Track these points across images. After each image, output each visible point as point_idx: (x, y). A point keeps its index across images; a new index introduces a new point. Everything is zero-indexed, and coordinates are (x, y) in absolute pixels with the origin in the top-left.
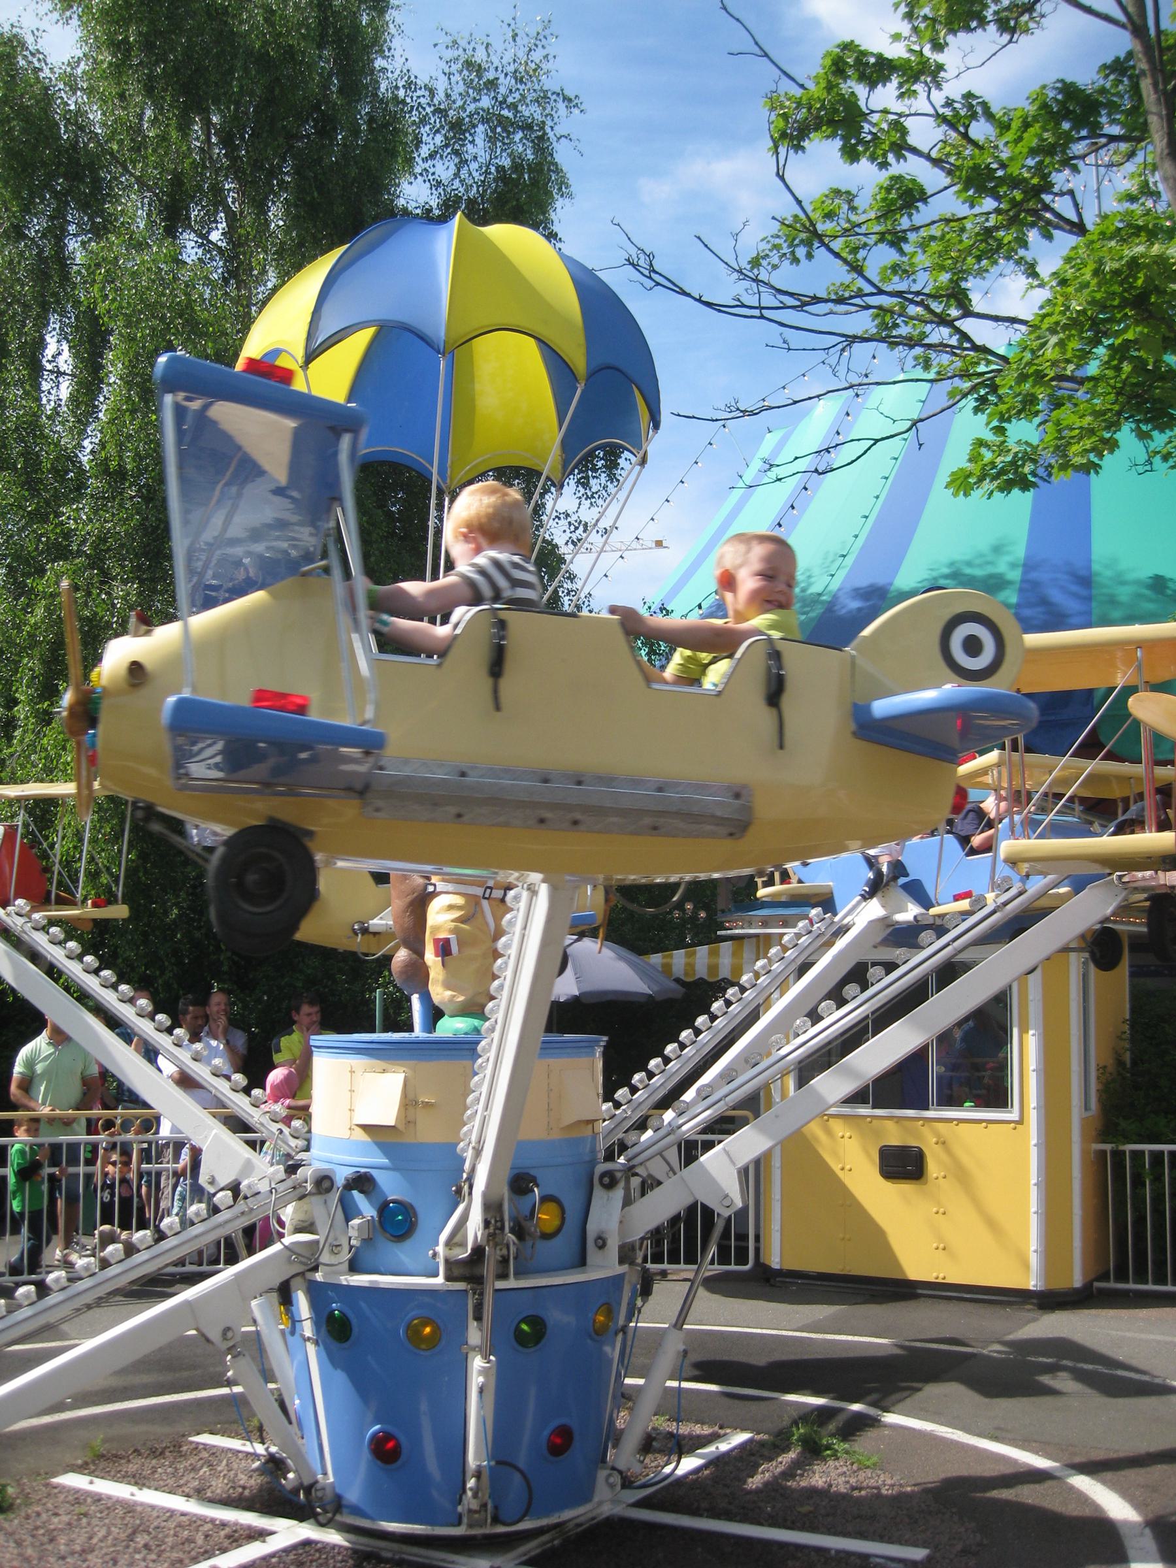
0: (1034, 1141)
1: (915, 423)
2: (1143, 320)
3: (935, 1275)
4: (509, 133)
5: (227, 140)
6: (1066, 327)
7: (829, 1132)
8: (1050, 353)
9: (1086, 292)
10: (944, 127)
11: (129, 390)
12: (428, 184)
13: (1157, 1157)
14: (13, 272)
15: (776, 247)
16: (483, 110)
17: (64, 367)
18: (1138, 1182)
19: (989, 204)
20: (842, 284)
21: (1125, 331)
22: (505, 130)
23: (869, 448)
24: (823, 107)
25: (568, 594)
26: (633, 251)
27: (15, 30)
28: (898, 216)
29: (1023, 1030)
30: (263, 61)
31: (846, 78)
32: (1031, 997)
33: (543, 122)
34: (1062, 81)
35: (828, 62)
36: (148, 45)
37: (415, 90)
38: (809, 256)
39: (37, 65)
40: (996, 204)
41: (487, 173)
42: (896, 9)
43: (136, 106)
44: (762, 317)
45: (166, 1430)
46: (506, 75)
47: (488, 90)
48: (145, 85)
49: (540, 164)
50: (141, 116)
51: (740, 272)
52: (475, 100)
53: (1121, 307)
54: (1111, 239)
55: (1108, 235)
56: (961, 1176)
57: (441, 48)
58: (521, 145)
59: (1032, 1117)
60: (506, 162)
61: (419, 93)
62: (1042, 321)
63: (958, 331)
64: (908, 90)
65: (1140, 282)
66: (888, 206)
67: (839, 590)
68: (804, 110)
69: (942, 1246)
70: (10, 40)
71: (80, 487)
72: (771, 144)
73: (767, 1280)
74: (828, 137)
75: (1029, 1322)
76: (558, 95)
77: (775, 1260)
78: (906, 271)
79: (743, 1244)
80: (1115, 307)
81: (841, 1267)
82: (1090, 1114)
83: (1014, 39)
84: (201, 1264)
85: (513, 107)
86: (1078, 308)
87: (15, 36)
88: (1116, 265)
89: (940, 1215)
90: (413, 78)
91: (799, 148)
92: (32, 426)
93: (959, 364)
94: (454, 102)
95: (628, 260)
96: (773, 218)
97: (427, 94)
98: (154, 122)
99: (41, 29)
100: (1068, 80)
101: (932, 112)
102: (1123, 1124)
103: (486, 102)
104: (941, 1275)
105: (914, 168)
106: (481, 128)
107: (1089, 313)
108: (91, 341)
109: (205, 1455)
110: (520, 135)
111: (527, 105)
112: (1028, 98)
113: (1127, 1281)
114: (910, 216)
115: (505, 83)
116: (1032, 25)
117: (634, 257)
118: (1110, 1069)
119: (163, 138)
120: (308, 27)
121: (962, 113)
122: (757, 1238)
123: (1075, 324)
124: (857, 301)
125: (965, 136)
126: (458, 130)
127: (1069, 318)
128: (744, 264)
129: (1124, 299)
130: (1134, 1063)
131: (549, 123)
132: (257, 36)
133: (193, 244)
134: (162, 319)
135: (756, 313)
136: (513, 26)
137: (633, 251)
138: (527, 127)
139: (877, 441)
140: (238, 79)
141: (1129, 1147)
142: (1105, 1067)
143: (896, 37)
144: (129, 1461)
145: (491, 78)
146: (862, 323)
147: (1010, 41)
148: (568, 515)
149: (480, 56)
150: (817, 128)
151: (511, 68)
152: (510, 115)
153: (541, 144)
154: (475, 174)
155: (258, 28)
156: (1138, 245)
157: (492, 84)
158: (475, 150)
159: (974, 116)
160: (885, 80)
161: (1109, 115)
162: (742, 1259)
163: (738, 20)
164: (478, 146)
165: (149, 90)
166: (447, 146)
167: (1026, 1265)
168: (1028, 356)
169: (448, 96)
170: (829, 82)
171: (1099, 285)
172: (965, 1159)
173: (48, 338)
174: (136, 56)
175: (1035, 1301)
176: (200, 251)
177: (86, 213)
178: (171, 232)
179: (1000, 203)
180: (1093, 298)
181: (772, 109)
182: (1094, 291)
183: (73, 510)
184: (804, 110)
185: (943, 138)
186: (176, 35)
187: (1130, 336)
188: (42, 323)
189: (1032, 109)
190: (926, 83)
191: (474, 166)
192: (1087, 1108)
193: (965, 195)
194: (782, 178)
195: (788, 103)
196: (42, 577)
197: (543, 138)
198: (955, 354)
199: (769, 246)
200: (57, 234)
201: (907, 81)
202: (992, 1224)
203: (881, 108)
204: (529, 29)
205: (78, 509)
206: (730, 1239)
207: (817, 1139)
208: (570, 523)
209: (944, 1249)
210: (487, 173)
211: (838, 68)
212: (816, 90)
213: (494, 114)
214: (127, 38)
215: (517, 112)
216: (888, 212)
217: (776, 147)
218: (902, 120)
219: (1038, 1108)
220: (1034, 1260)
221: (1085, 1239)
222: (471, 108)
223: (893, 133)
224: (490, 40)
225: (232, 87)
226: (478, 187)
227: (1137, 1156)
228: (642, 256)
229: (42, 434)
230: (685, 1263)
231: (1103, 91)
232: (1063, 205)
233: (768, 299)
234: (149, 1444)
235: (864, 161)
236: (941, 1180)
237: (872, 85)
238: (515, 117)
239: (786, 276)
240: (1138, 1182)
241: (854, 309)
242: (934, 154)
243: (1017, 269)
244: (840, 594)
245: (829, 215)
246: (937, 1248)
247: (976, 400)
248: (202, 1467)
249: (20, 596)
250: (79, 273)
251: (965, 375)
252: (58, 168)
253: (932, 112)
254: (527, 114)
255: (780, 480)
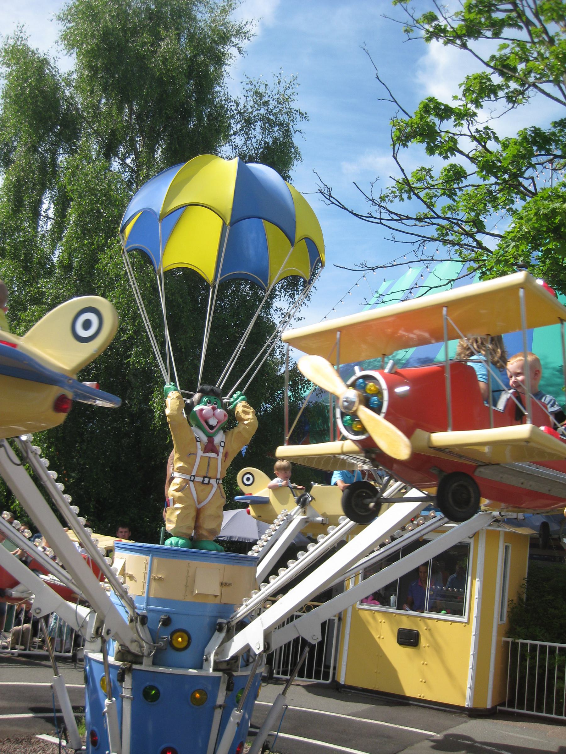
0: (473, 633)
1: (450, 281)
2: (557, 238)
3: (419, 695)
4: (272, 127)
5: (139, 118)
6: (519, 239)
7: (374, 619)
8: (510, 250)
9: (530, 223)
10: (475, 143)
11: (77, 228)
12: (231, 147)
13: (534, 647)
14: (30, 167)
15: (393, 192)
16: (261, 115)
17: (51, 215)
18: (523, 659)
19: (492, 180)
20: (423, 213)
21: (549, 243)
22: (270, 125)
23: (427, 291)
24: (418, 127)
25: (279, 347)
26: (322, 186)
27: (45, 57)
28: (452, 184)
29: (473, 578)
30: (160, 82)
31: (430, 114)
32: (478, 562)
33: (289, 124)
34: (534, 127)
35: (422, 106)
36: (106, 69)
37: (230, 102)
38: (409, 198)
39: (54, 73)
40: (496, 180)
41: (260, 144)
42: (460, 87)
43: (97, 96)
44: (381, 223)
45: (26, 730)
46: (273, 99)
47: (264, 106)
48: (103, 87)
49: (286, 143)
50: (99, 102)
51: (373, 201)
52: (257, 110)
53: (547, 232)
54: (546, 200)
55: (545, 198)
56: (437, 648)
57: (244, 84)
58: (277, 133)
59: (474, 621)
60: (270, 141)
61: (232, 104)
62: (508, 235)
63: (476, 240)
64: (459, 122)
65: (557, 221)
66: (448, 178)
67: (410, 358)
68: (409, 128)
69: (424, 681)
70: (42, 60)
71: (50, 273)
72: (392, 143)
73: (337, 689)
74: (420, 142)
75: (463, 723)
76: (297, 111)
77: (342, 680)
78: (454, 210)
79: (327, 670)
80: (544, 231)
81: (374, 686)
82: (502, 622)
83: (515, 107)
84: (61, 652)
85: (275, 115)
86: (526, 230)
87: (45, 59)
88: (546, 211)
89: (424, 665)
90: (229, 97)
91: (405, 145)
92: (30, 242)
93: (473, 255)
94: (248, 109)
95: (319, 190)
96: (390, 177)
97: (235, 105)
98: (106, 104)
99: (58, 57)
100: (537, 127)
101: (469, 134)
102: (519, 629)
103: (263, 111)
104: (422, 695)
105: (457, 160)
106: (259, 123)
107: (532, 233)
108: (63, 204)
109: (42, 745)
110: (277, 128)
111: (282, 115)
112: (518, 134)
113: (514, 708)
114: (458, 184)
115: (272, 104)
116: (524, 101)
117: (323, 189)
118: (515, 601)
119: (110, 113)
120: (183, 68)
121: (484, 136)
122: (335, 668)
123: (524, 237)
124: (427, 220)
125: (484, 147)
126: (248, 123)
127: (521, 235)
128: (376, 197)
129: (548, 228)
130: (527, 600)
131: (291, 124)
132: (158, 70)
133: (118, 164)
134: (96, 195)
135: (378, 221)
136: (279, 77)
137: (322, 186)
138: (281, 125)
139: (431, 288)
140: (147, 89)
141: (520, 641)
142: (512, 600)
143: (455, 98)
144: (4, 744)
145: (266, 100)
146: (432, 231)
147: (513, 107)
148: (281, 309)
149: (262, 90)
150: (415, 137)
151: (276, 97)
152: (274, 118)
153: (287, 133)
154: (254, 144)
155: (159, 66)
156: (557, 203)
157: (266, 103)
158: (255, 133)
159: (489, 138)
160: (448, 117)
161: (556, 145)
162: (326, 677)
163: (384, 84)
164: (257, 131)
165: (105, 89)
166: (242, 130)
167: (464, 696)
168: (502, 252)
169: (245, 106)
170: (421, 115)
171: (537, 220)
172: (440, 641)
173: (45, 201)
174: (101, 73)
175: (467, 713)
176: (120, 167)
177: (68, 143)
178: (107, 156)
179: (498, 180)
180: (534, 226)
181: (394, 125)
182: (534, 223)
183: (45, 282)
184: (409, 128)
185: (476, 148)
186: (120, 65)
187: (550, 246)
188: (41, 193)
189: (519, 139)
190: (467, 120)
191: (254, 140)
192: (501, 620)
193: (481, 174)
194: (395, 158)
195: (402, 124)
196: (25, 312)
197: (288, 130)
198: (473, 251)
199: (390, 192)
200: (54, 154)
201: (459, 119)
202: (449, 674)
203: (446, 130)
204: (286, 78)
205: (47, 282)
206: (321, 667)
207: (368, 622)
208: (282, 314)
209: (425, 682)
210: (260, 144)
211: (426, 109)
212: (416, 119)
213: (266, 117)
214: (97, 64)
215: (277, 117)
216: (448, 181)
217: (394, 145)
218: (456, 137)
219: (477, 617)
220: (468, 692)
221: (494, 685)
222: (255, 113)
223: (450, 143)
224: (267, 83)
225: (143, 92)
226: (255, 150)
227: (524, 645)
228: (326, 189)
229: (35, 245)
230: (307, 677)
231: (554, 134)
232: (526, 183)
233: (385, 215)
234: (16, 736)
235: (436, 155)
236: (427, 648)
237: (442, 119)
238: (276, 119)
239: (398, 207)
240: (523, 659)
241: (426, 224)
242: (470, 155)
243: (508, 213)
244: (411, 361)
245: (419, 180)
246: (421, 682)
247: (481, 273)
248: (39, 751)
249: (15, 320)
250: (63, 171)
251: (476, 260)
252: (57, 121)
253: (469, 134)
254: (282, 119)
255: (384, 302)
